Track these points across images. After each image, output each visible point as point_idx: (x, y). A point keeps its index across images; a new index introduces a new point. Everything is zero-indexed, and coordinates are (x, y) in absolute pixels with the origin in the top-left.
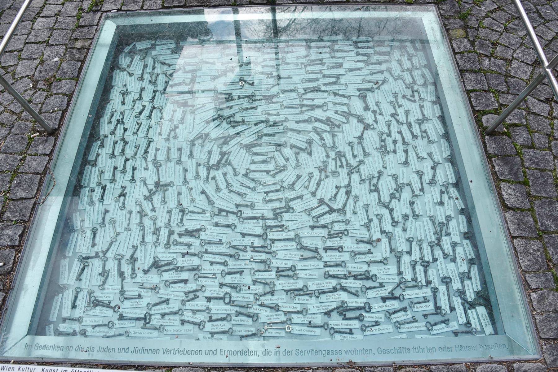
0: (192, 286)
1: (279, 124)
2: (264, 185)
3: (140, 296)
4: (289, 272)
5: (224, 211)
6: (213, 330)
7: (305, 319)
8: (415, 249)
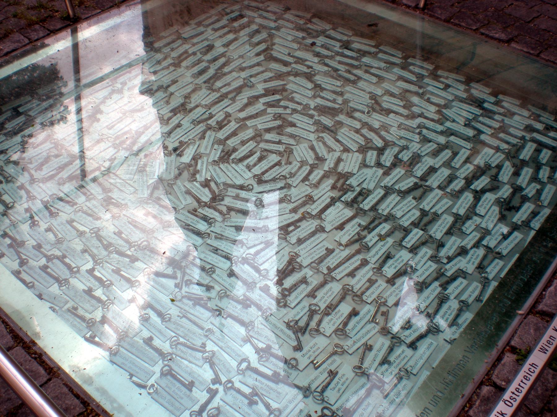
0: (367, 311)
1: (225, 122)
2: (292, 175)
3: (333, 374)
4: (426, 220)
5: (289, 225)
6: (449, 320)
7: (496, 236)
8: (319, 147)
